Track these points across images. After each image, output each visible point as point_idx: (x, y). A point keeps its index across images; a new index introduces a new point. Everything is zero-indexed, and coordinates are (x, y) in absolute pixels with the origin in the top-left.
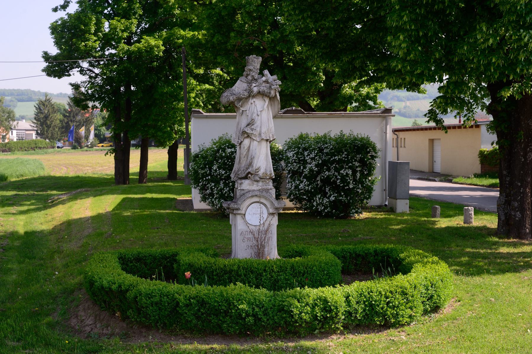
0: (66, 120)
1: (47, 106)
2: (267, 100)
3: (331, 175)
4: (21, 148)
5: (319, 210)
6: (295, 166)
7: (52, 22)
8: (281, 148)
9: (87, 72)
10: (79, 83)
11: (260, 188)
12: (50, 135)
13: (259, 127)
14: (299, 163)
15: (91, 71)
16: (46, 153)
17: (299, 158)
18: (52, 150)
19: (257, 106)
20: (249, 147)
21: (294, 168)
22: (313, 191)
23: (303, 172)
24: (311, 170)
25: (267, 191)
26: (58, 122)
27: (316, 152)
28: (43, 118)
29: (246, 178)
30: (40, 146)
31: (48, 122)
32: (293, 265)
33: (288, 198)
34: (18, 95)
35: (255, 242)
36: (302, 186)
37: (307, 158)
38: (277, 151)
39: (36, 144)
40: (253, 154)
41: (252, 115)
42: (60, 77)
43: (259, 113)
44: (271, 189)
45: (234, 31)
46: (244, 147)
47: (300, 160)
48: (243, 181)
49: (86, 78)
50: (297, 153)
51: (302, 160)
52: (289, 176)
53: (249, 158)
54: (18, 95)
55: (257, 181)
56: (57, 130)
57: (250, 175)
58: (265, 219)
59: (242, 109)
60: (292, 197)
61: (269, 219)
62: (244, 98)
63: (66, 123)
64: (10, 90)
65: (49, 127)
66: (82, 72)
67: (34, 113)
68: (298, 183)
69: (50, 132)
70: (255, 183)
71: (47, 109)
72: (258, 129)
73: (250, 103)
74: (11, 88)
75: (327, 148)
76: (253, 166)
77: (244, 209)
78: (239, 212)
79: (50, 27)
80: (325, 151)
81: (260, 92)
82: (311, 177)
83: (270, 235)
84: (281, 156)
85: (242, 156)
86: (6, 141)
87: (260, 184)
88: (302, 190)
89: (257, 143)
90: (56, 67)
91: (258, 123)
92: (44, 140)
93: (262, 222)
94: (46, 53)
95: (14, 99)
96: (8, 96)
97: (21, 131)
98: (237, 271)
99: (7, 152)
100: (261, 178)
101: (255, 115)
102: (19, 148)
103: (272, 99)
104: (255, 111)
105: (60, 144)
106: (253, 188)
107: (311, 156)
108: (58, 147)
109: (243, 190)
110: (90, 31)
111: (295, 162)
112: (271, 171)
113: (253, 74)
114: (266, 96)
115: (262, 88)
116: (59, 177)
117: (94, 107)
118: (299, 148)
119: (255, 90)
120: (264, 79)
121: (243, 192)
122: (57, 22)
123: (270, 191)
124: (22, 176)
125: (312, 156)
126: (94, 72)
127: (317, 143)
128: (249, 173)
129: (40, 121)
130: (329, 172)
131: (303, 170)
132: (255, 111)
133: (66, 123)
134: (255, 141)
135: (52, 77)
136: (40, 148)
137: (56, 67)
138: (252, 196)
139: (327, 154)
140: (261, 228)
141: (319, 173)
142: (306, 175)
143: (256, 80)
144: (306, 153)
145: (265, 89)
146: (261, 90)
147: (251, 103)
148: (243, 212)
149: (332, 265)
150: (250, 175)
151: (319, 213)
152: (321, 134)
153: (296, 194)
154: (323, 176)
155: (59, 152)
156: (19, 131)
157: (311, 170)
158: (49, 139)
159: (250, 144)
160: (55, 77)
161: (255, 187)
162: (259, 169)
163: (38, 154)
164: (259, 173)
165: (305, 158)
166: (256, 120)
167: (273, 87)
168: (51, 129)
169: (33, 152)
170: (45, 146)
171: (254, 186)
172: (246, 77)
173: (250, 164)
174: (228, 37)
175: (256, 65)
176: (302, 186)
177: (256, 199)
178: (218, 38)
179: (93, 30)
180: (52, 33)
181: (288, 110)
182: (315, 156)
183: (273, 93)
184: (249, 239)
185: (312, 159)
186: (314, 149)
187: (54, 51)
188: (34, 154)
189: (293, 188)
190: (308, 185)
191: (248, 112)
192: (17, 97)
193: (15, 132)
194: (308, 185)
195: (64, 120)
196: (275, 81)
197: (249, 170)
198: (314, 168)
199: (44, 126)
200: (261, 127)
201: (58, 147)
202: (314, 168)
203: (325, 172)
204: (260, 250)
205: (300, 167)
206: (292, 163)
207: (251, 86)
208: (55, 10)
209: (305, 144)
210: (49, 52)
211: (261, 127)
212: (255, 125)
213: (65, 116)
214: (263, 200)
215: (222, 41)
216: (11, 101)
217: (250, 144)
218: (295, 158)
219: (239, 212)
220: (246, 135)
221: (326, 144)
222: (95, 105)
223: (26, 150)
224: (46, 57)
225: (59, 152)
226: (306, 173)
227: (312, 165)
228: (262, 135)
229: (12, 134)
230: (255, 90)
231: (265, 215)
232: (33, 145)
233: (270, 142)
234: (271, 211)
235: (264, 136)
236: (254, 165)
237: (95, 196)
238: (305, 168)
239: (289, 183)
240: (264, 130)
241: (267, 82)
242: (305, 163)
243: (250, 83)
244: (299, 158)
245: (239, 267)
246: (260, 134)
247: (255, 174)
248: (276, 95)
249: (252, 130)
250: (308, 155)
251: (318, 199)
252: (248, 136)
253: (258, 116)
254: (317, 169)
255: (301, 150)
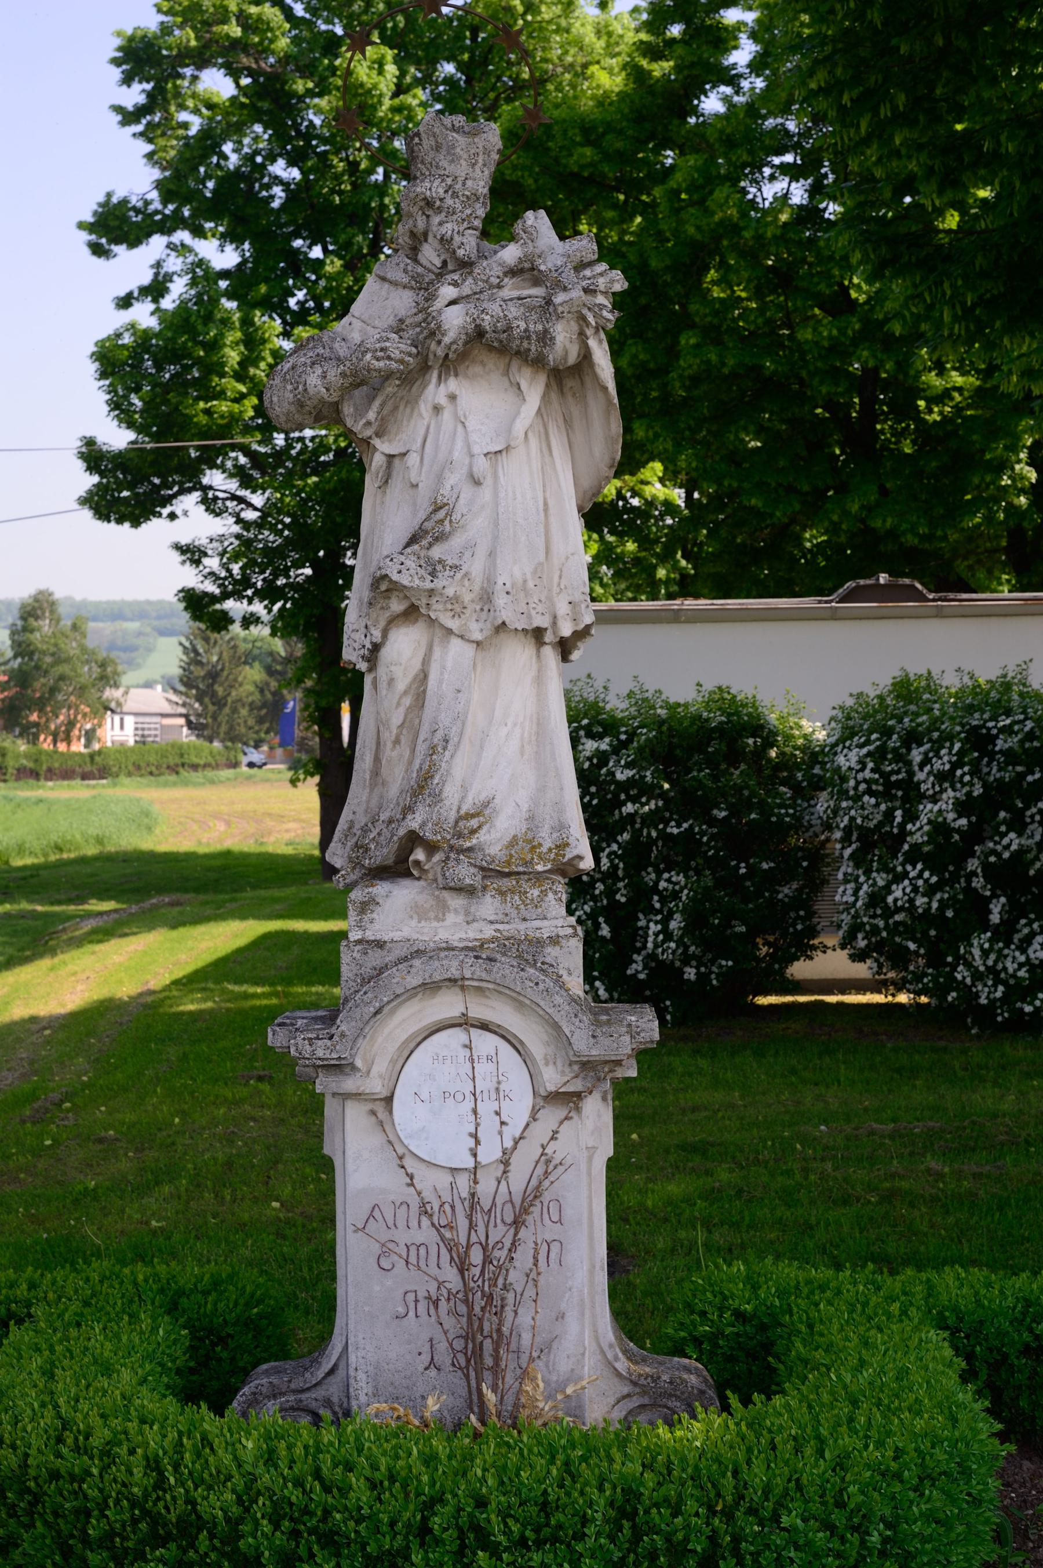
0: (274, 684)
1: (216, 642)
2: (534, 390)
3: (1029, 850)
4: (138, 768)
5: (983, 1001)
6: (871, 810)
7: (103, 335)
8: (821, 735)
9: (228, 503)
10: (204, 541)
11: (489, 932)
12: (224, 728)
13: (481, 552)
14: (886, 795)
15: (241, 500)
16: (212, 782)
17: (885, 776)
18: (229, 773)
19: (471, 424)
20: (423, 676)
21: (865, 818)
22: (950, 914)
23: (903, 834)
24: (940, 828)
25: (528, 952)
26: (251, 688)
27: (957, 746)
28: (204, 678)
29: (398, 869)
30: (195, 760)
31: (220, 690)
32: (631, 1494)
33: (843, 947)
34: (159, 618)
35: (451, 1276)
36: (898, 894)
37: (920, 776)
38: (804, 749)
39: (182, 755)
40: (445, 720)
41: (440, 478)
42: (136, 523)
43: (482, 465)
44: (555, 940)
45: (692, 326)
46: (391, 681)
47: (889, 785)
48: (381, 889)
49: (225, 526)
50: (879, 755)
51: (898, 784)
52: (847, 852)
53: (421, 748)
54: (159, 618)
55: (469, 891)
56: (244, 712)
57: (419, 855)
58: (514, 1129)
59: (384, 446)
60: (862, 943)
61: (541, 1131)
62: (387, 376)
63: (274, 694)
64: (138, 603)
65: (220, 703)
66: (211, 505)
67: (177, 663)
68: (881, 883)
69: (223, 718)
70: (456, 902)
71: (217, 649)
72: (476, 567)
73: (424, 408)
74: (141, 597)
75: (1008, 730)
76: (437, 798)
77: (381, 1066)
78: (350, 1084)
79: (93, 354)
80: (1000, 744)
81: (480, 333)
82: (945, 852)
83: (550, 1231)
84: (817, 770)
85: (388, 737)
86: (96, 746)
87: (488, 906)
88: (898, 910)
89: (469, 650)
90: (126, 490)
91: (474, 527)
92: (206, 744)
93: (490, 1153)
94: (90, 442)
95: (148, 630)
96: (132, 620)
97: (147, 719)
98: (234, 1523)
99: (94, 778)
100: (488, 872)
101: (454, 479)
102: (131, 768)
103: (567, 378)
104: (458, 453)
105: (255, 756)
106: (443, 935)
107: (938, 765)
108: (251, 765)
109: (380, 944)
110: (223, 365)
111: (870, 792)
112: (562, 827)
113: (448, 228)
114: (522, 355)
115: (495, 308)
116: (166, 853)
117: (250, 620)
118: (887, 732)
119: (454, 321)
120: (511, 253)
121: (376, 958)
122: (118, 335)
123: (551, 953)
124: (59, 849)
125: (942, 764)
126: (250, 505)
127: (970, 709)
128: (413, 839)
129: (197, 688)
130: (1020, 835)
131: (902, 826)
132: (458, 453)
133: (274, 694)
134: (455, 643)
135: (113, 524)
136: (195, 767)
137: (126, 490)
138: (430, 987)
139: (1010, 757)
140: (486, 1187)
141: (974, 836)
142: (916, 847)
143: (466, 265)
144: (916, 755)
145: (513, 311)
146: (487, 321)
147: (437, 409)
148: (376, 1086)
149: (926, 1477)
150: (419, 855)
151: (985, 1014)
152: (987, 673)
153: (875, 930)
154: (994, 852)
155: (249, 778)
156: (141, 719)
157: (940, 828)
158: (222, 741)
159: (426, 662)
160: (120, 521)
161: (456, 926)
162: (482, 812)
163: (186, 784)
164: (483, 836)
165: (911, 774)
166: (461, 507)
167: (559, 298)
168: (227, 710)
169: (173, 778)
170: (210, 760)
171: (451, 918)
172: (414, 252)
173: (423, 786)
174: (673, 352)
175: (462, 169)
176: (898, 894)
177: (449, 1005)
178: (635, 356)
179: (233, 356)
180: (103, 375)
181: (858, 587)
182: (955, 766)
183: (563, 335)
184: (413, 1257)
185: (942, 777)
186: (950, 738)
187: (118, 438)
188: (175, 784)
189: (859, 903)
190: (931, 891)
191: (413, 459)
192: (156, 623)
193: (130, 721)
194: (931, 891)
195: (267, 684)
196: (580, 266)
197: (413, 823)
198: (951, 816)
199: (207, 700)
200: (492, 554)
201: (251, 765)
202: (951, 816)
203: (1004, 835)
204: (480, 1331)
205: (889, 815)
206: (857, 798)
207: (431, 298)
208: (125, 302)
209: (917, 715)
210: (100, 439)
211: (492, 554)
212: (456, 542)
213: (270, 671)
214: (478, 1011)
215: (652, 365)
216: (139, 634)
217: (426, 662)
218: (867, 774)
219: (350, 1084)
220: (397, 606)
221: (1008, 713)
222: (252, 614)
223: (151, 773)
224: (93, 456)
225: (249, 778)
226: (918, 838)
227: (943, 807)
228: (501, 600)
229: (122, 727)
230: (454, 321)
231: (519, 1106)
232: (173, 760)
233: (565, 648)
234: (553, 1078)
235: (506, 610)
236: (451, 794)
237: (174, 927)
238: (911, 816)
239: (846, 881)
240: (512, 569)
241: (526, 271)
242: (911, 795)
243: (424, 288)
244: (885, 776)
245: (246, 1500)
246: (486, 598)
247: (458, 840)
248: (586, 356)
249: (433, 569)
250: (926, 761)
251: (976, 952)
252: (411, 613)
253: (477, 483)
254: (963, 821)
255: (894, 742)
